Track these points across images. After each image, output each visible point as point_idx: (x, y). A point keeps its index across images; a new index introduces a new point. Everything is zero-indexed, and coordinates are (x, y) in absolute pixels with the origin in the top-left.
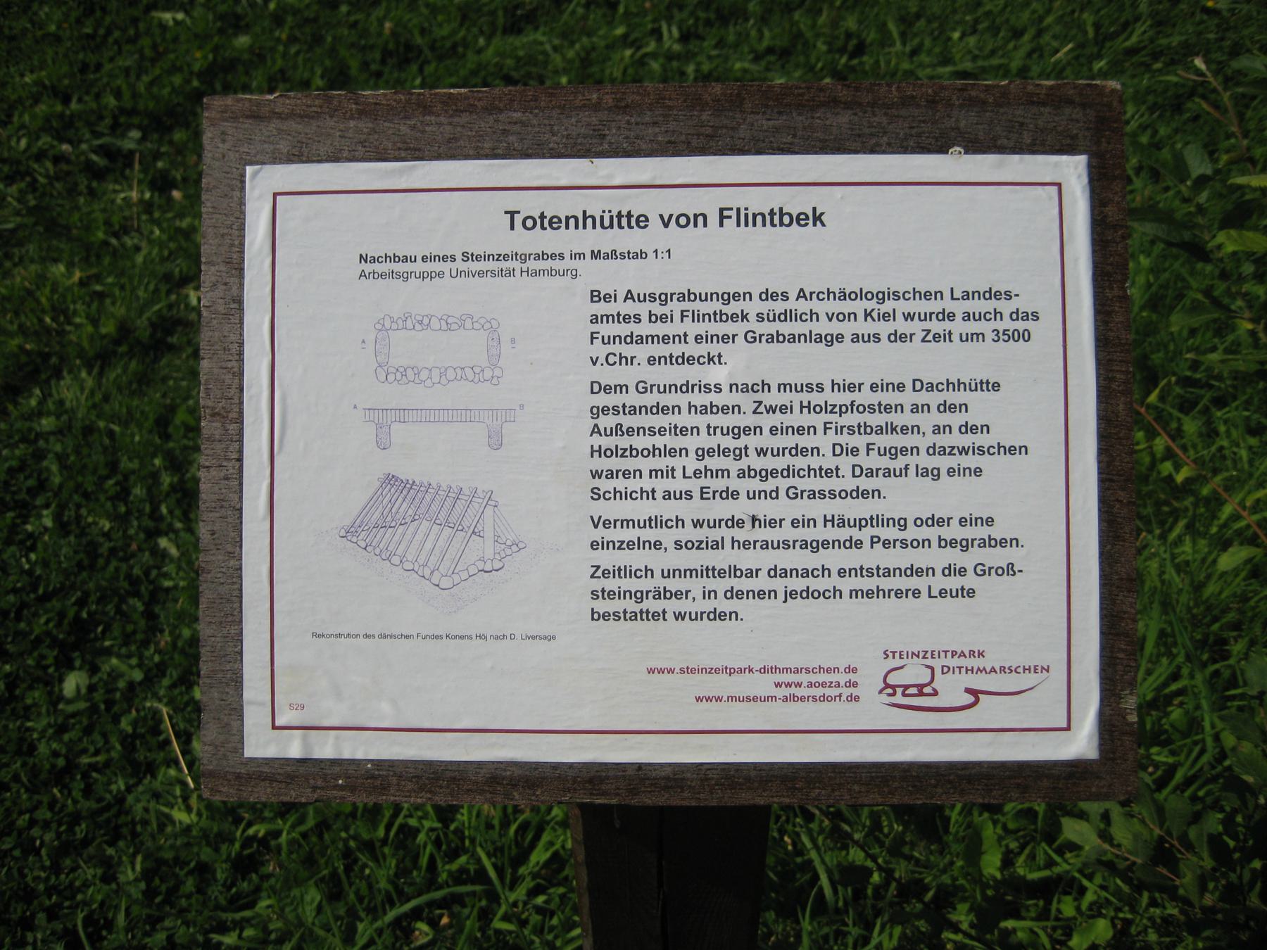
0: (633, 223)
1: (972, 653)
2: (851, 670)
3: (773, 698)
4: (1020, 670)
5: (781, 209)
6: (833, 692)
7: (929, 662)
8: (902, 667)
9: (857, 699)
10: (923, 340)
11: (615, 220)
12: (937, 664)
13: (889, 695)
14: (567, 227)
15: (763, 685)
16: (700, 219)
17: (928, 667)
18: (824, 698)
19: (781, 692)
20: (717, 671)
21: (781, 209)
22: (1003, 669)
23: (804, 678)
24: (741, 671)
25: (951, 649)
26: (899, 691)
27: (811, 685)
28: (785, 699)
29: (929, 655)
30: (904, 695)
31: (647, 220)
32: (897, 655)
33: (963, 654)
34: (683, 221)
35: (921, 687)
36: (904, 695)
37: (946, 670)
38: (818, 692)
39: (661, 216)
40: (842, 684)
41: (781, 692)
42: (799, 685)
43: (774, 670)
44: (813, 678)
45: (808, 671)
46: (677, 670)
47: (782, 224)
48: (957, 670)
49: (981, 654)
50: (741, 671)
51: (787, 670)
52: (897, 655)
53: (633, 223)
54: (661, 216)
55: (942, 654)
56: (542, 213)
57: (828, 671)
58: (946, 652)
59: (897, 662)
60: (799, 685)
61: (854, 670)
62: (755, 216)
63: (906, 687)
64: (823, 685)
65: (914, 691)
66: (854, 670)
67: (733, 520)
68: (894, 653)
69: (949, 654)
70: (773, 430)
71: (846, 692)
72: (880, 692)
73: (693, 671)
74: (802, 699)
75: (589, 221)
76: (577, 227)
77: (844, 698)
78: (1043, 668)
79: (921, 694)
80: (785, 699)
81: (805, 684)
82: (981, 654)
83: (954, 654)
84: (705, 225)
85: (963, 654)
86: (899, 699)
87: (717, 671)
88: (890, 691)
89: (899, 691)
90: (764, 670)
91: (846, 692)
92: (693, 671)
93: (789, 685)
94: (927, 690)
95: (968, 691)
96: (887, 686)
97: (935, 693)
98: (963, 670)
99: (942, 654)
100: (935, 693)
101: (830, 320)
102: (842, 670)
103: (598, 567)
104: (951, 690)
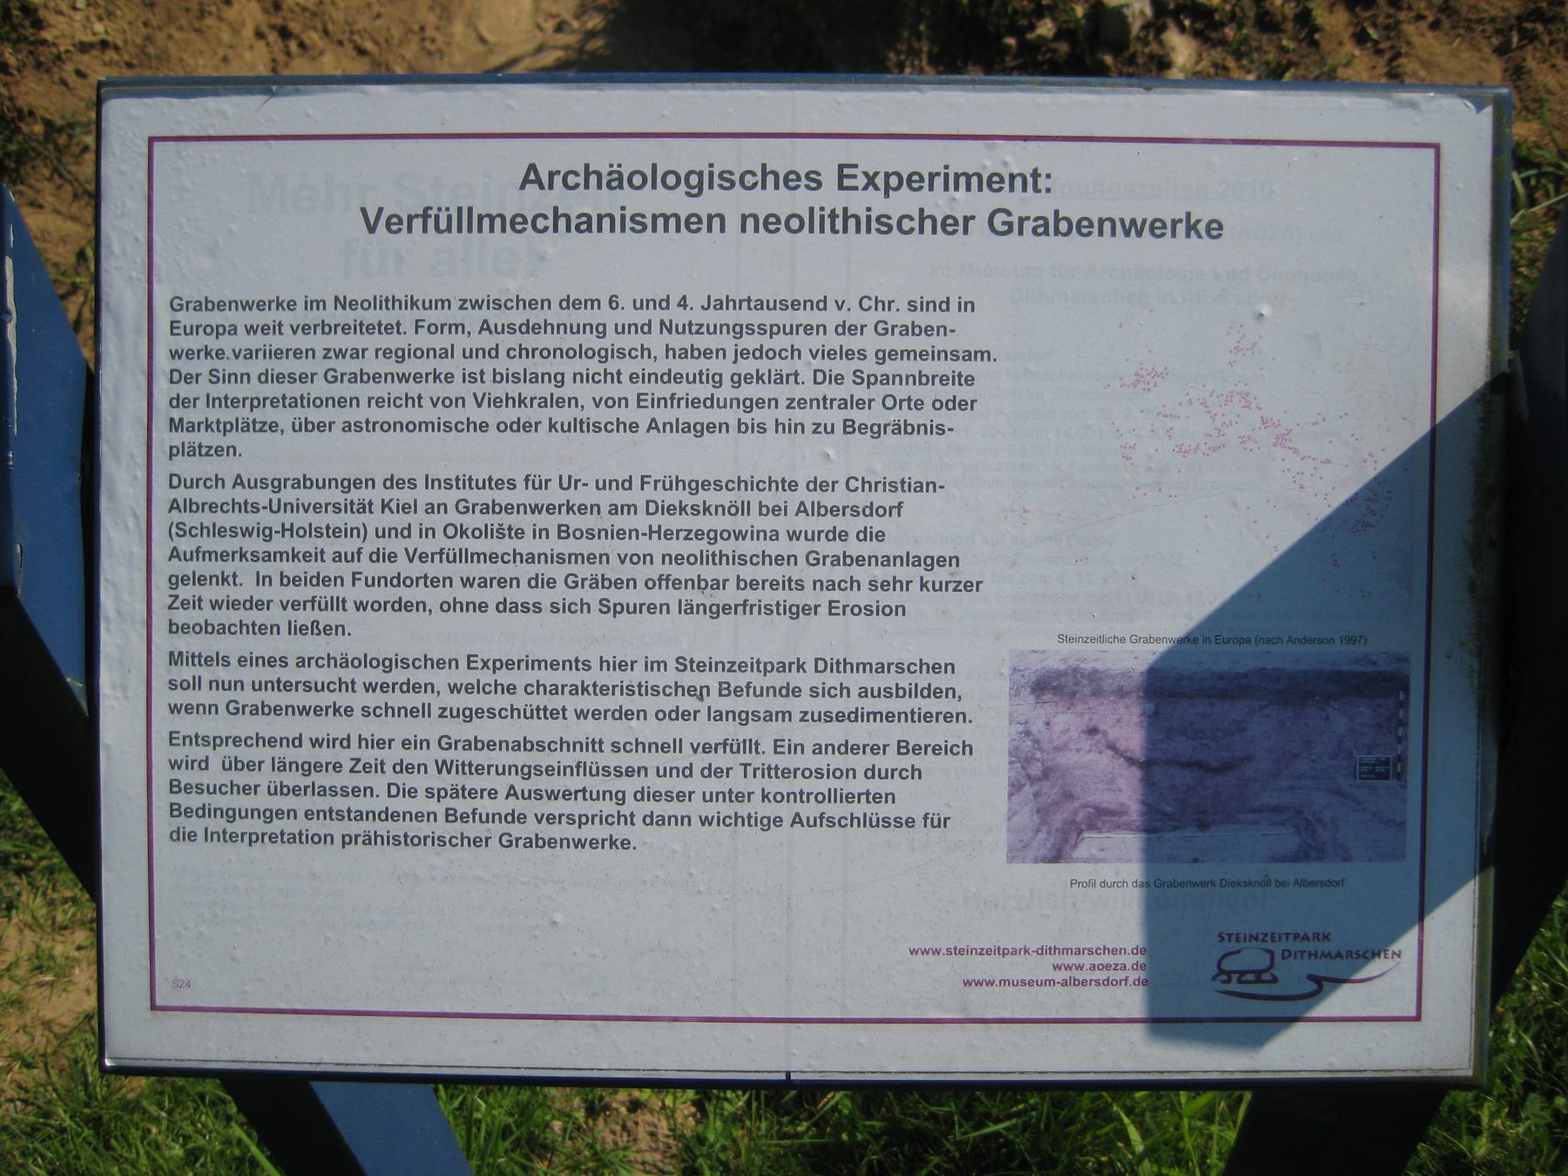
1: (1316, 936)
3: (1051, 982)
5: (845, 210)
6: (1120, 975)
7: (1269, 945)
8: (1238, 952)
10: (352, 771)
11: (827, 222)
12: (1277, 948)
14: (710, 229)
15: (1042, 968)
16: (716, 222)
18: (1107, 982)
19: (1060, 976)
20: (989, 952)
21: (845, 210)
23: (1086, 960)
24: (1015, 952)
25: (1292, 930)
26: (1235, 977)
27: (1093, 967)
28: (1065, 983)
31: (1221, 227)
33: (1306, 937)
34: (610, 403)
35: (1258, 973)
36: (1240, 981)
39: (364, 211)
42: (1080, 967)
43: (1053, 950)
44: (1097, 960)
47: (1057, 232)
49: (1326, 937)
50: (1015, 952)
51: (1067, 951)
54: (364, 211)
57: (1114, 952)
59: (1233, 946)
60: (1080, 967)
62: (481, 218)
63: (1242, 973)
64: (1107, 967)
65: (1250, 977)
68: (1230, 935)
72: (1214, 978)
73: (961, 952)
74: (1084, 983)
75: (852, 222)
76: (612, 229)
79: (1259, 980)
80: (1065, 983)
82: (1326, 937)
83: (1296, 936)
84: (722, 229)
85: (1306, 937)
86: (1234, 986)
87: (989, 952)
88: (1224, 977)
89: (1235, 977)
90: (1041, 951)
92: (961, 952)
93: (1069, 967)
94: (1266, 976)
95: (1310, 977)
96: (1221, 972)
97: (1275, 980)
100: (1275, 980)
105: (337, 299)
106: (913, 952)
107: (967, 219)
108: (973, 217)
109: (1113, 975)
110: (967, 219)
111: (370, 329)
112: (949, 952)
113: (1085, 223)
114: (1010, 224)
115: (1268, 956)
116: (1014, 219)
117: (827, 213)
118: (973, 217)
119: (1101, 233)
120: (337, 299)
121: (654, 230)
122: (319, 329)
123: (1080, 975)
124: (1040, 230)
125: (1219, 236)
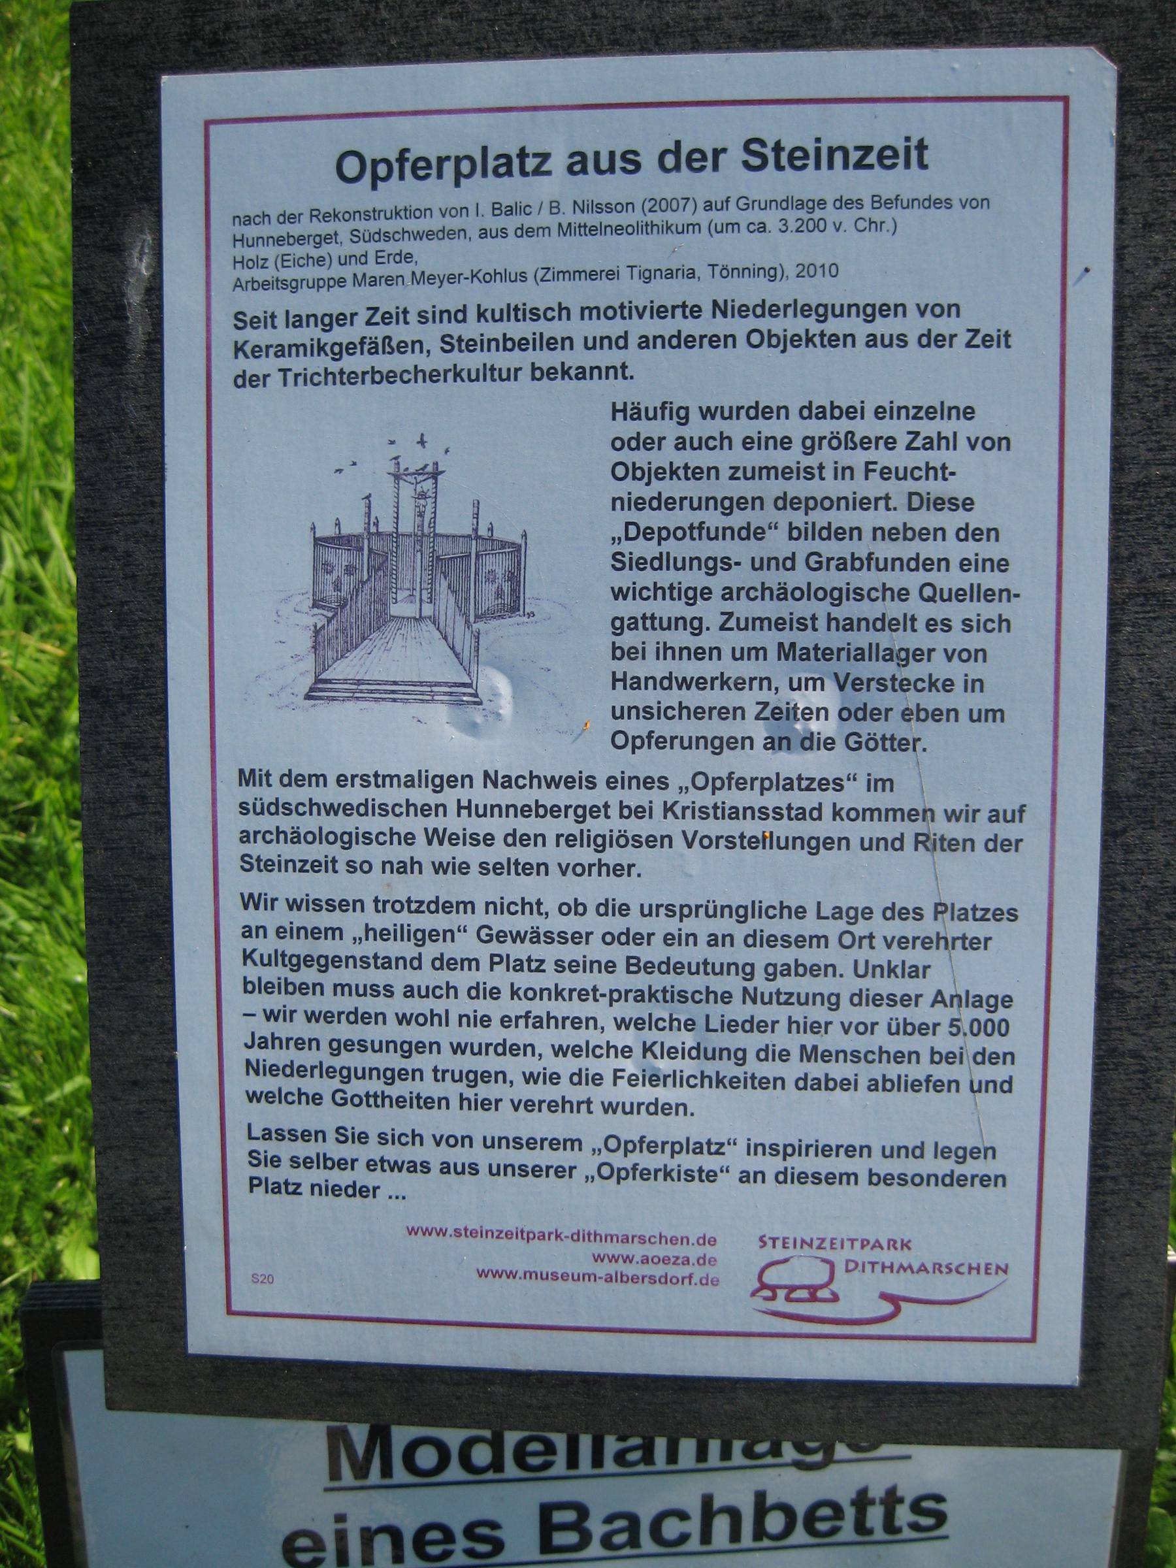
0: (784, 160)
1: (892, 1244)
2: (704, 1240)
3: (591, 1277)
4: (964, 1269)
7: (827, 1254)
8: (786, 1261)
9: (715, 1282)
12: (839, 1257)
13: (766, 1299)
15: (578, 1257)
17: (824, 1261)
18: (665, 1280)
19: (603, 1269)
22: (938, 1267)
23: (637, 1250)
24: (542, 1236)
26: (781, 1293)
27: (645, 1260)
28: (609, 1279)
29: (827, 1244)
30: (788, 1299)
32: (779, 1243)
33: (878, 1245)
35: (813, 1290)
37: (852, 1265)
38: (658, 1270)
40: (693, 1260)
41: (603, 1269)
42: (628, 1259)
45: (642, 1240)
46: (450, 1231)
48: (868, 1267)
49: (905, 1245)
50: (542, 1236)
52: (779, 1243)
53: (784, 160)
55: (847, 1244)
56: (778, 143)
57: (673, 1241)
58: (852, 1241)
59: (779, 1253)
60: (628, 1259)
61: (712, 1242)
63: (792, 1289)
64: (665, 1260)
65: (804, 1294)
66: (712, 1242)
67: (756, 408)
68: (774, 1240)
69: (857, 1245)
70: (747, 443)
71: (699, 1272)
72: (753, 1294)
73: (473, 1234)
74: (634, 1279)
77: (695, 1280)
78: (998, 1267)
79: (813, 1298)
80: (609, 1279)
81: (638, 1258)
82: (905, 1245)
83: (864, 1243)
85: (878, 1245)
86: (780, 1305)
87: (509, 1235)
89: (781, 1293)
90: (577, 1237)
91: (699, 1272)
93: (614, 1259)
94: (823, 1294)
95: (884, 1296)
97: (835, 1298)
98: (878, 1268)
99: (847, 1244)
100: (835, 1298)
101: (438, 1144)
102: (693, 1240)
103: (976, 332)
104: (859, 1296)
105: (715, 303)
106: (412, 1231)
107: (717, 153)
108: (724, 150)
109: (672, 1270)
110: (717, 153)
111: (522, 344)
112: (457, 1233)
113: (798, 154)
114: (820, 563)
115: (828, 1266)
116: (824, 560)
117: (914, 143)
118: (724, 150)
119: (896, 315)
120: (715, 303)
121: (612, 154)
122: (368, 378)
123: (629, 1270)
124: (577, 168)
125: (572, 155)
